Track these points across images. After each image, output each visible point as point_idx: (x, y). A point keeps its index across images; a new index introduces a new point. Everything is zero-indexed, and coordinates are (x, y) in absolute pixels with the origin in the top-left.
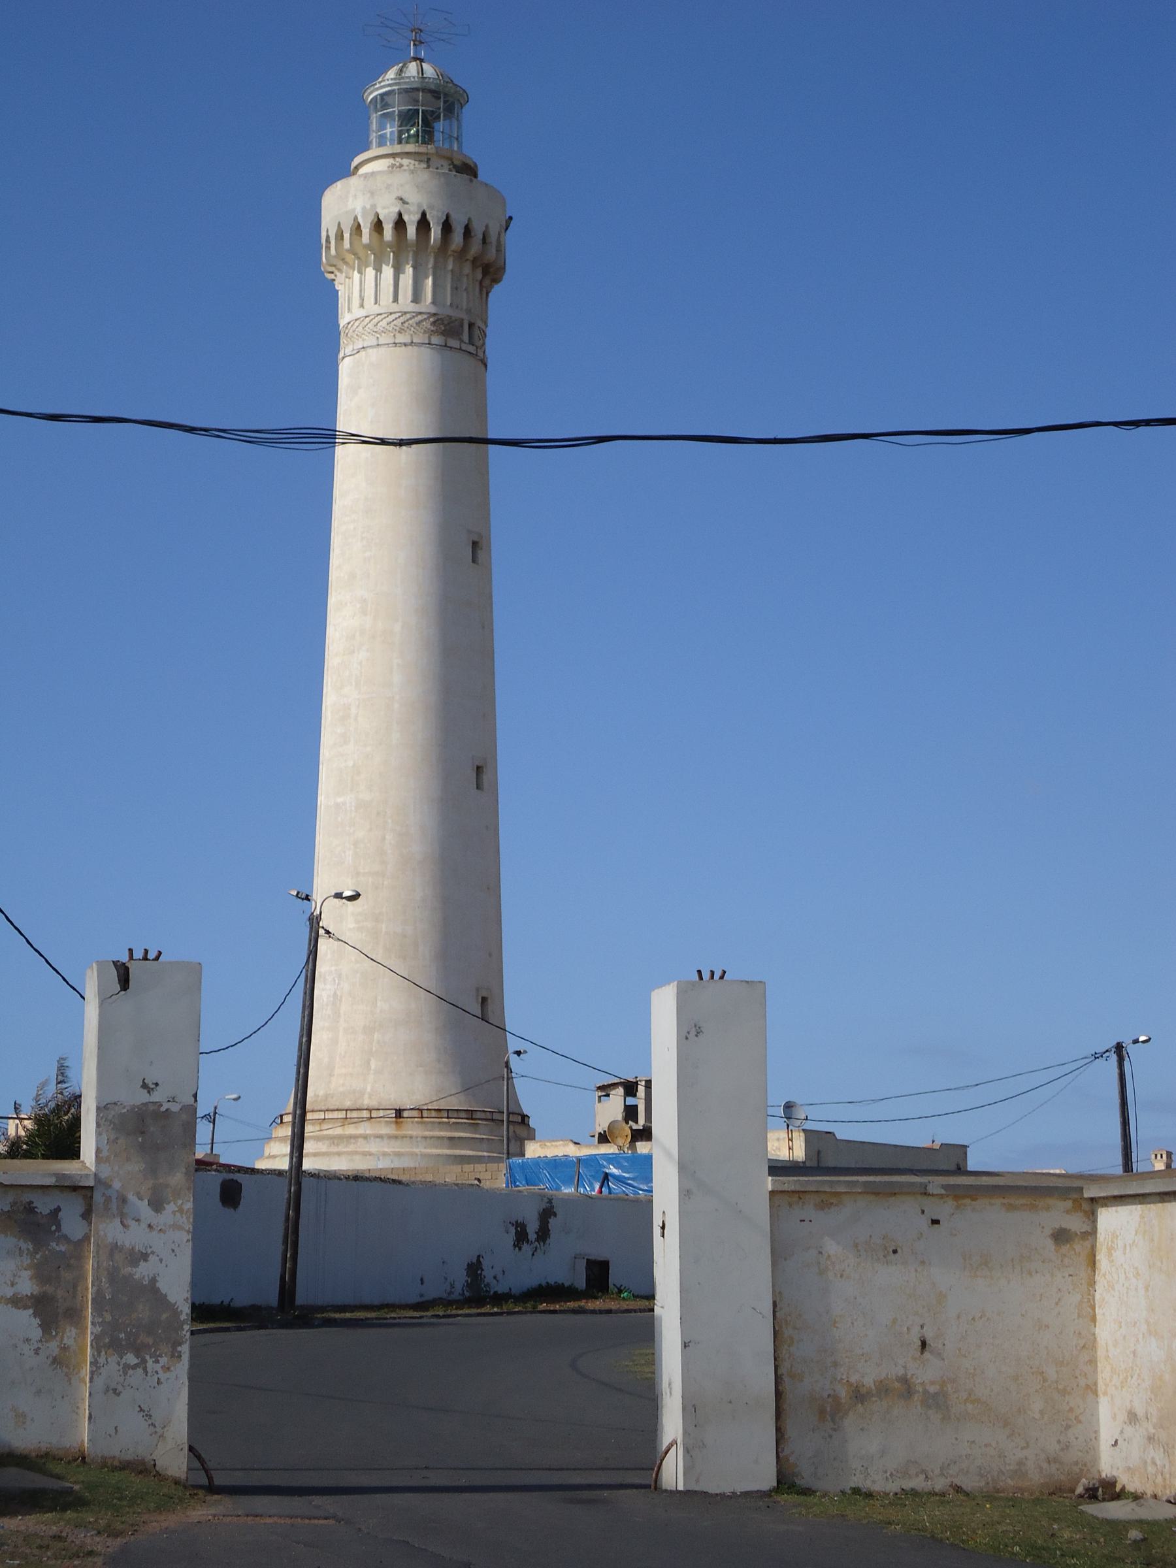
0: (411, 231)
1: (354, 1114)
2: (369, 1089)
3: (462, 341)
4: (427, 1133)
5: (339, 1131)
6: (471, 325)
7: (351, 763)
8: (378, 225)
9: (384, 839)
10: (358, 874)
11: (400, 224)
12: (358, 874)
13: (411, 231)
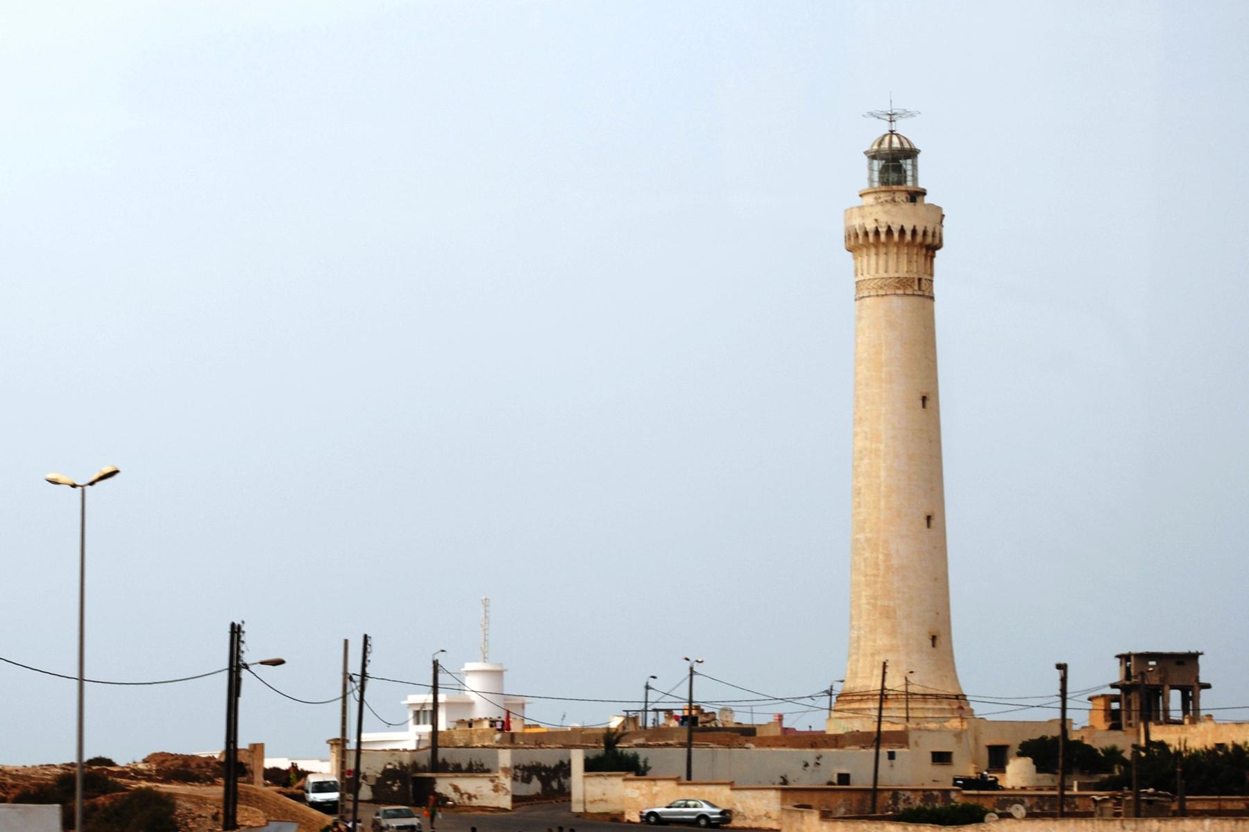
6: (920, 280)
11: (877, 233)
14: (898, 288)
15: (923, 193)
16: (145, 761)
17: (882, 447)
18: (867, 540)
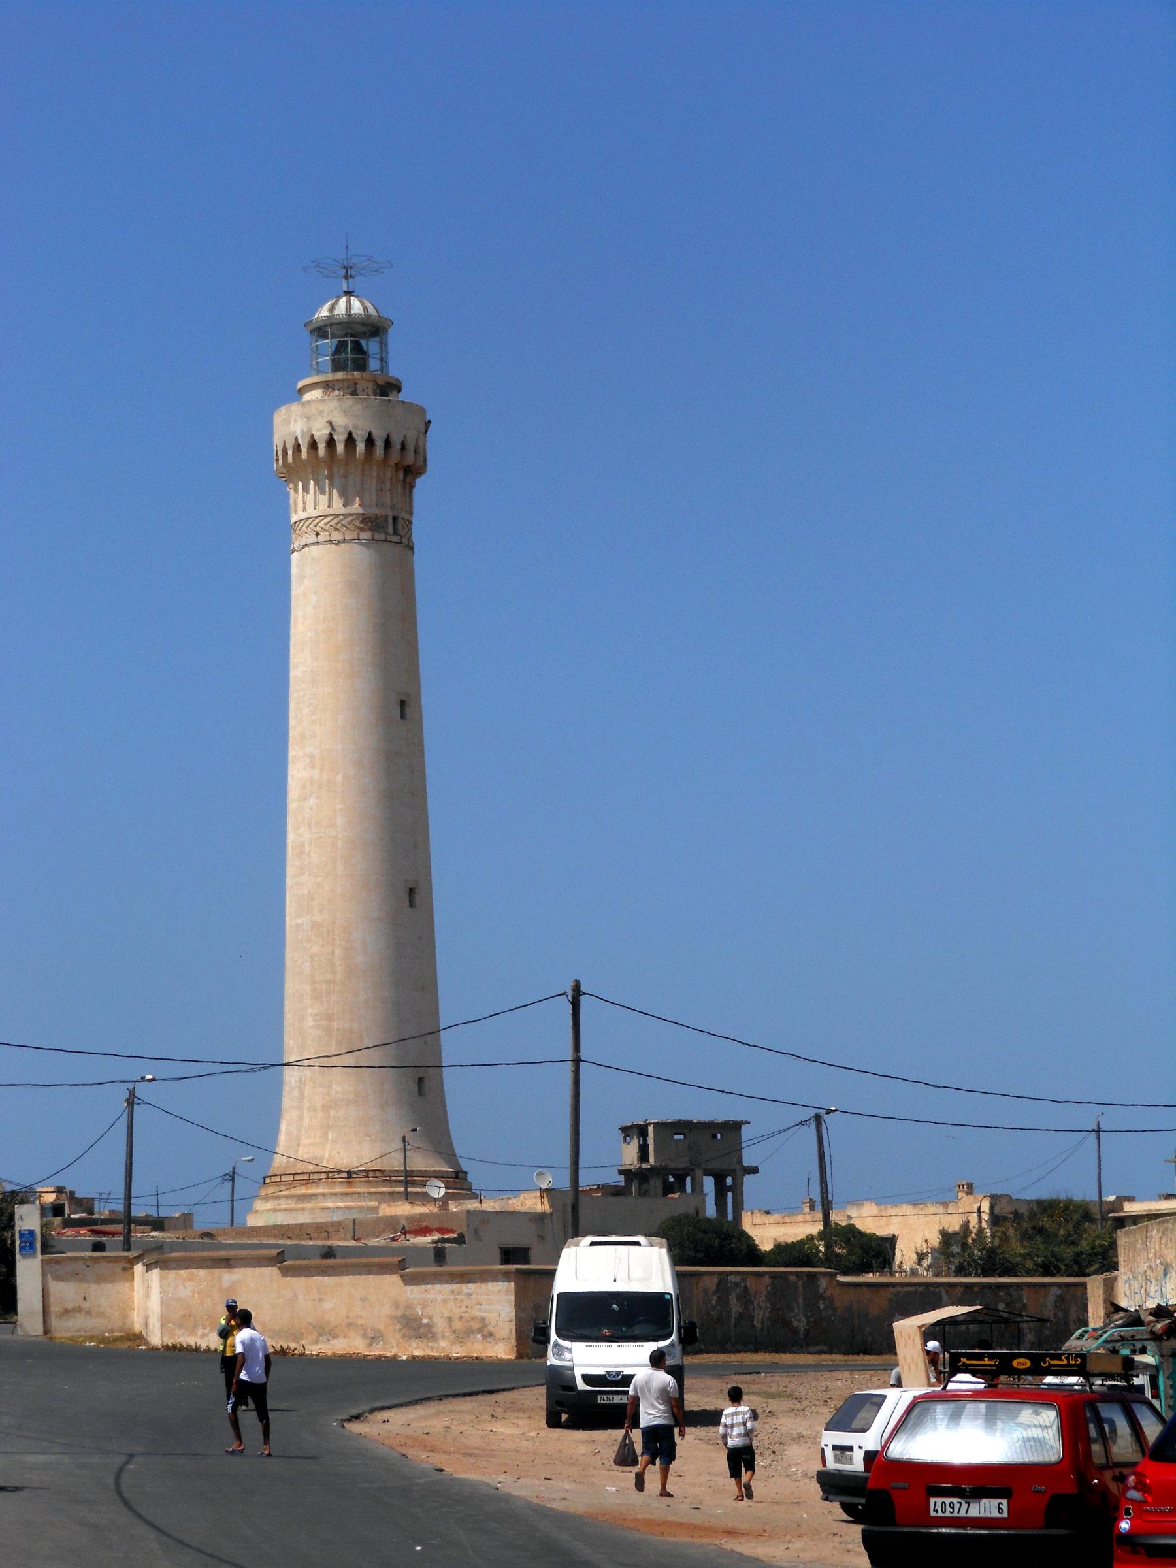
0: (340, 448)
1: (316, 1176)
2: (327, 1156)
3: (386, 533)
4: (372, 1190)
5: (302, 1191)
6: (395, 519)
7: (306, 891)
8: (313, 445)
9: (333, 953)
10: (314, 982)
11: (331, 443)
12: (314, 982)
13: (340, 448)
14: (362, 529)
15: (395, 386)
16: (587, 1379)
17: (339, 778)
18: (315, 926)
